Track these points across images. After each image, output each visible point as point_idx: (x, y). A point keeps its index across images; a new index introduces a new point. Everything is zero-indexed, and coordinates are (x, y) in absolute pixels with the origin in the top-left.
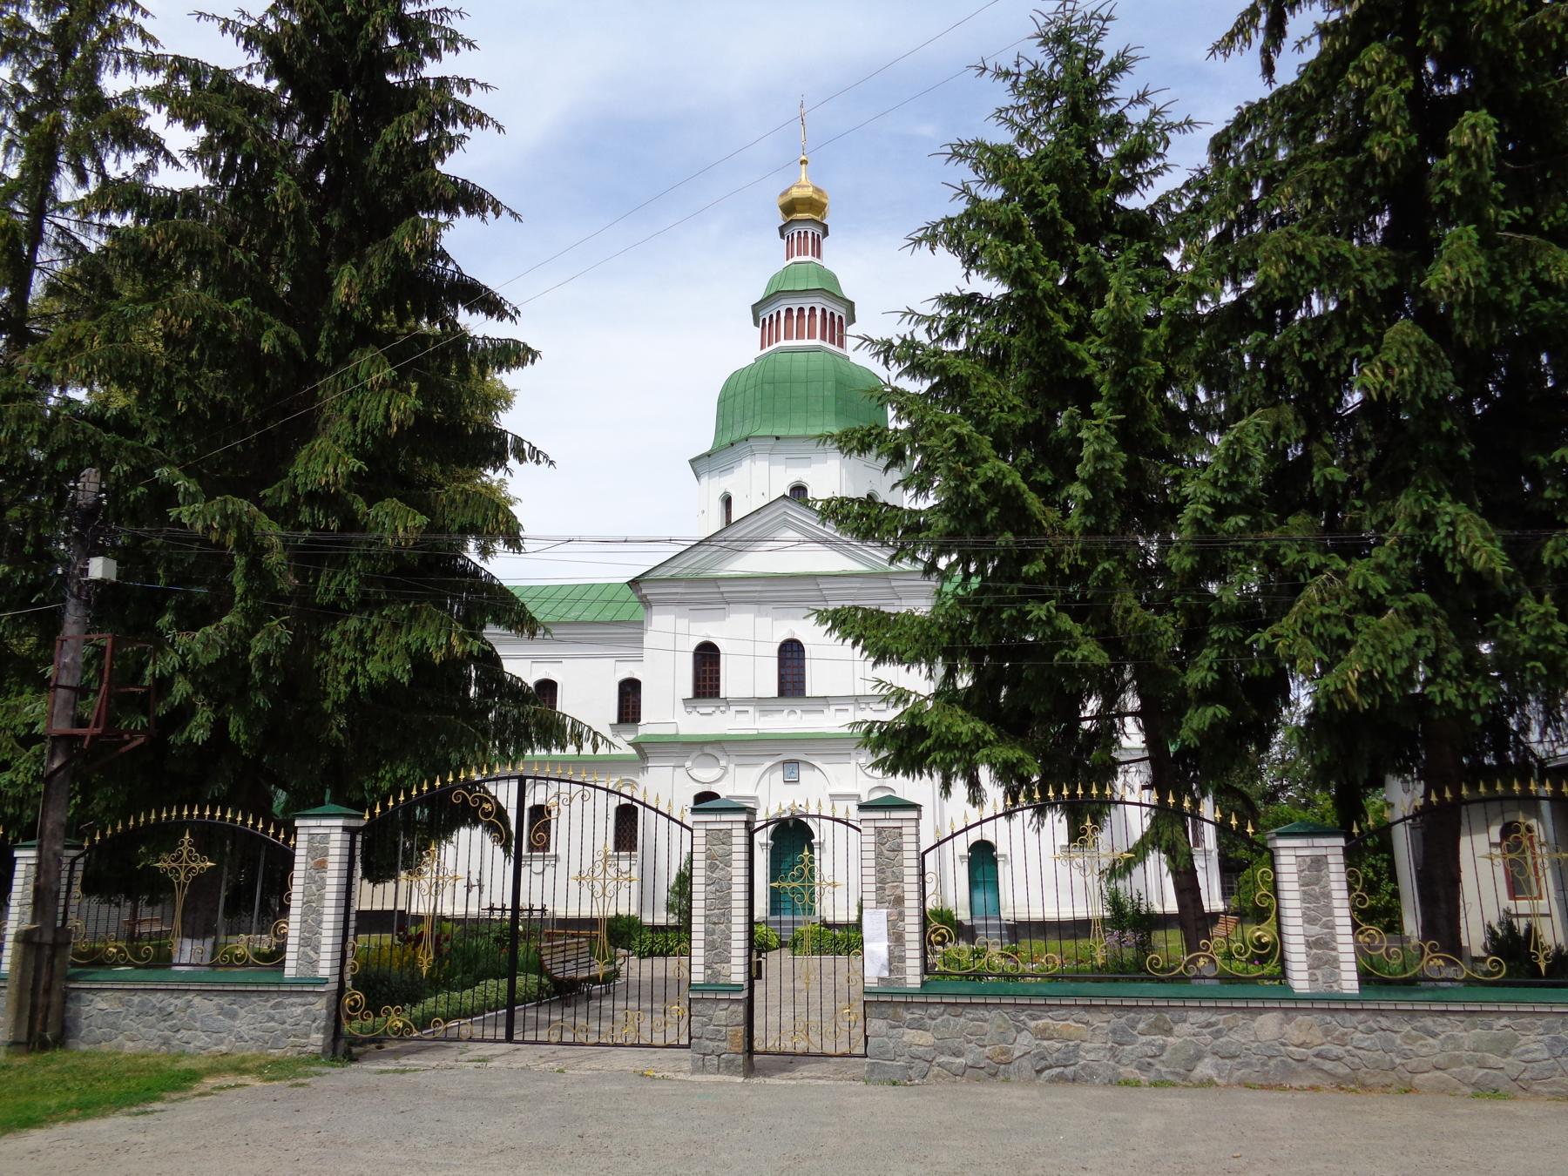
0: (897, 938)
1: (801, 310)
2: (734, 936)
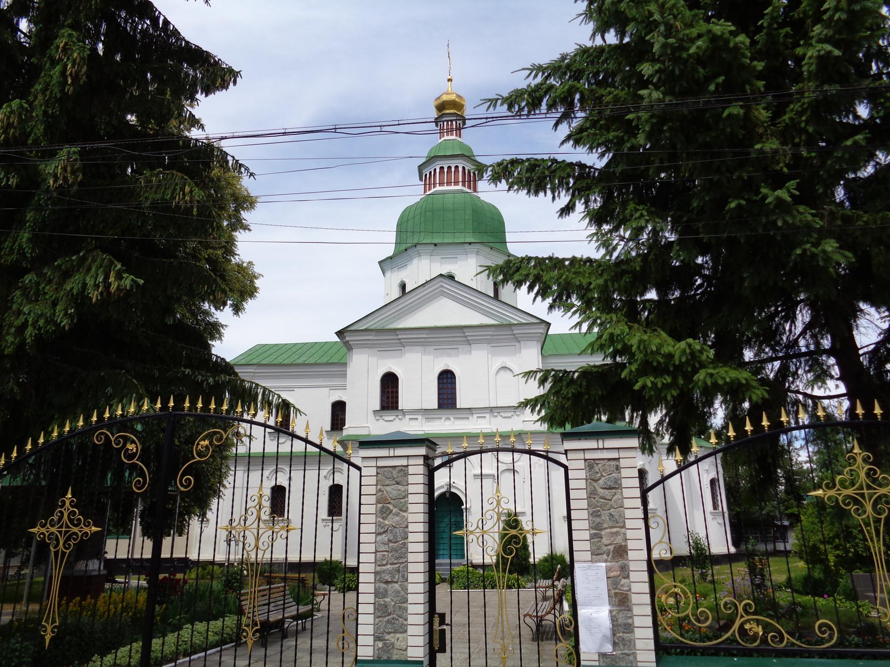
0: (621, 600)
1: (449, 168)
2: (411, 599)
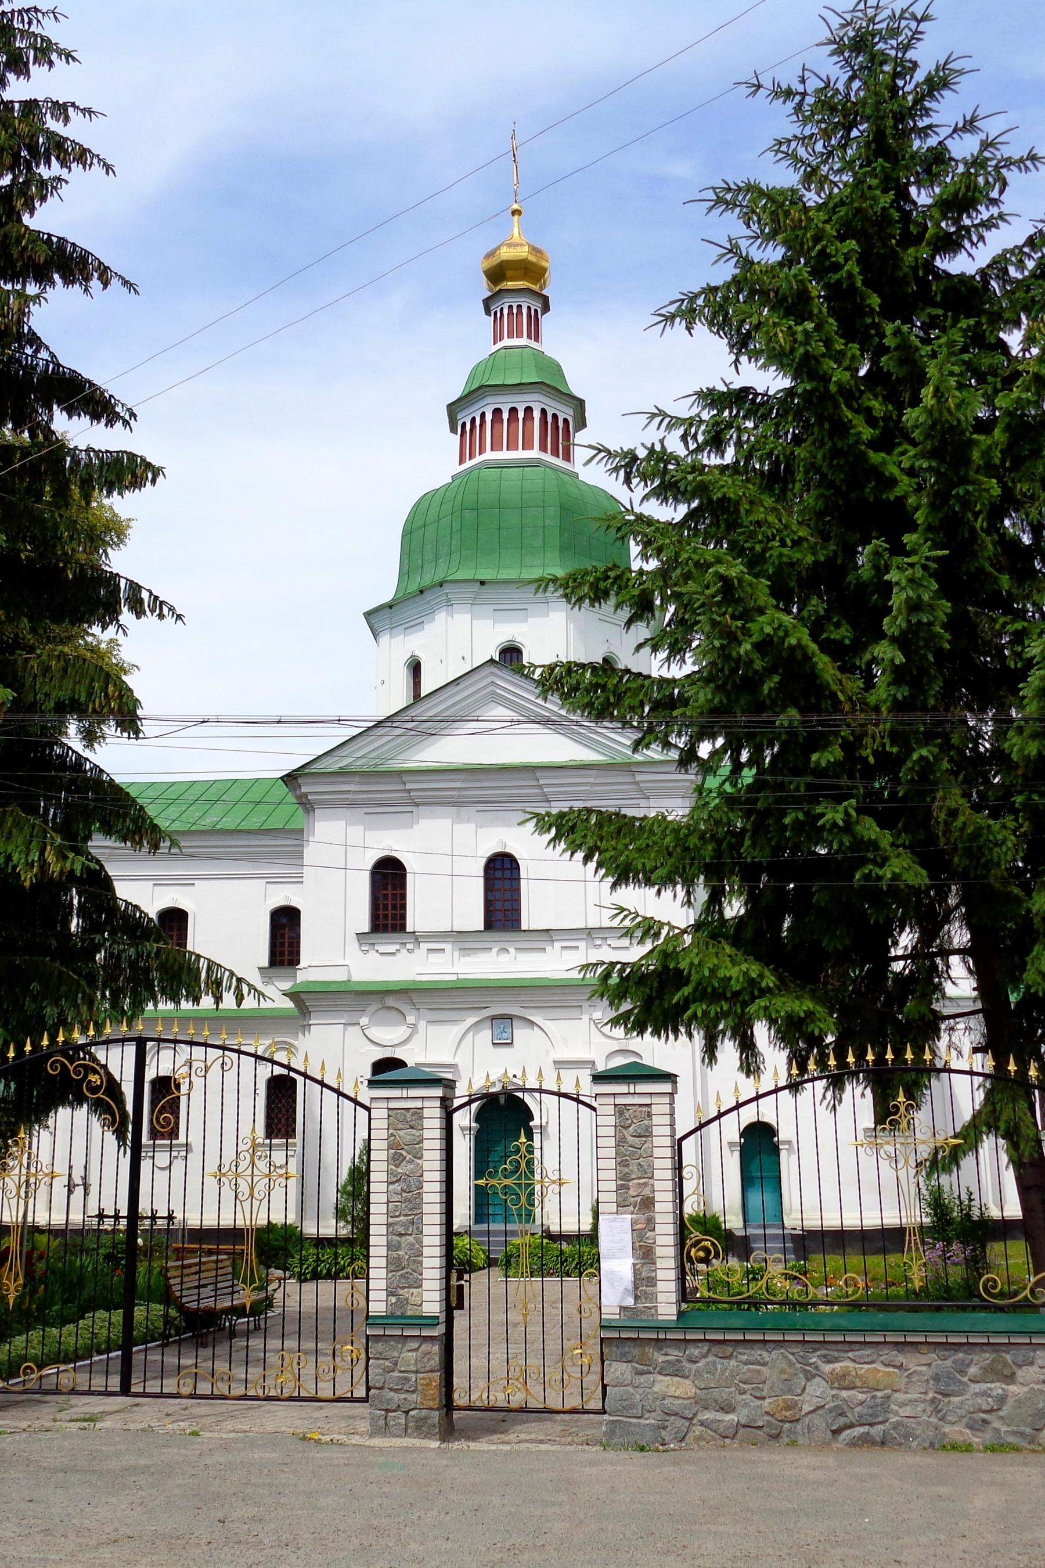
0: (645, 1253)
1: (513, 411)
2: (426, 1251)
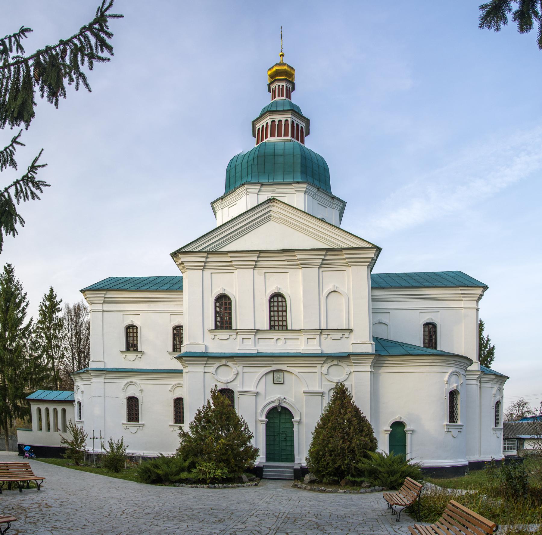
1: (280, 121)
